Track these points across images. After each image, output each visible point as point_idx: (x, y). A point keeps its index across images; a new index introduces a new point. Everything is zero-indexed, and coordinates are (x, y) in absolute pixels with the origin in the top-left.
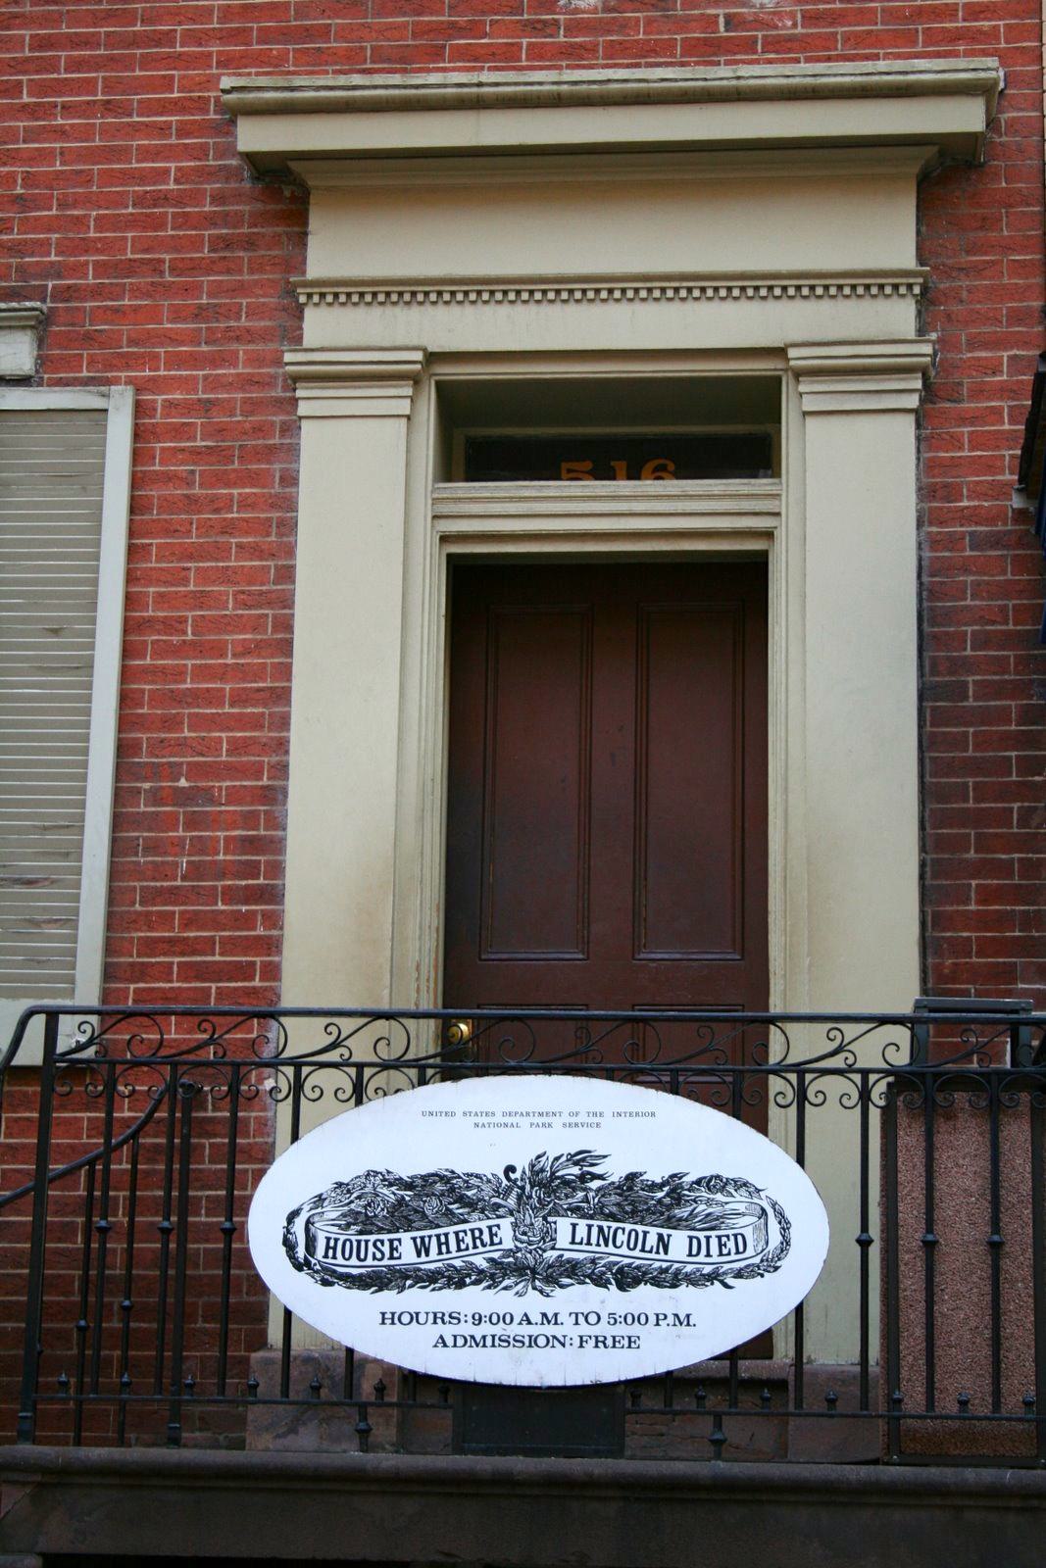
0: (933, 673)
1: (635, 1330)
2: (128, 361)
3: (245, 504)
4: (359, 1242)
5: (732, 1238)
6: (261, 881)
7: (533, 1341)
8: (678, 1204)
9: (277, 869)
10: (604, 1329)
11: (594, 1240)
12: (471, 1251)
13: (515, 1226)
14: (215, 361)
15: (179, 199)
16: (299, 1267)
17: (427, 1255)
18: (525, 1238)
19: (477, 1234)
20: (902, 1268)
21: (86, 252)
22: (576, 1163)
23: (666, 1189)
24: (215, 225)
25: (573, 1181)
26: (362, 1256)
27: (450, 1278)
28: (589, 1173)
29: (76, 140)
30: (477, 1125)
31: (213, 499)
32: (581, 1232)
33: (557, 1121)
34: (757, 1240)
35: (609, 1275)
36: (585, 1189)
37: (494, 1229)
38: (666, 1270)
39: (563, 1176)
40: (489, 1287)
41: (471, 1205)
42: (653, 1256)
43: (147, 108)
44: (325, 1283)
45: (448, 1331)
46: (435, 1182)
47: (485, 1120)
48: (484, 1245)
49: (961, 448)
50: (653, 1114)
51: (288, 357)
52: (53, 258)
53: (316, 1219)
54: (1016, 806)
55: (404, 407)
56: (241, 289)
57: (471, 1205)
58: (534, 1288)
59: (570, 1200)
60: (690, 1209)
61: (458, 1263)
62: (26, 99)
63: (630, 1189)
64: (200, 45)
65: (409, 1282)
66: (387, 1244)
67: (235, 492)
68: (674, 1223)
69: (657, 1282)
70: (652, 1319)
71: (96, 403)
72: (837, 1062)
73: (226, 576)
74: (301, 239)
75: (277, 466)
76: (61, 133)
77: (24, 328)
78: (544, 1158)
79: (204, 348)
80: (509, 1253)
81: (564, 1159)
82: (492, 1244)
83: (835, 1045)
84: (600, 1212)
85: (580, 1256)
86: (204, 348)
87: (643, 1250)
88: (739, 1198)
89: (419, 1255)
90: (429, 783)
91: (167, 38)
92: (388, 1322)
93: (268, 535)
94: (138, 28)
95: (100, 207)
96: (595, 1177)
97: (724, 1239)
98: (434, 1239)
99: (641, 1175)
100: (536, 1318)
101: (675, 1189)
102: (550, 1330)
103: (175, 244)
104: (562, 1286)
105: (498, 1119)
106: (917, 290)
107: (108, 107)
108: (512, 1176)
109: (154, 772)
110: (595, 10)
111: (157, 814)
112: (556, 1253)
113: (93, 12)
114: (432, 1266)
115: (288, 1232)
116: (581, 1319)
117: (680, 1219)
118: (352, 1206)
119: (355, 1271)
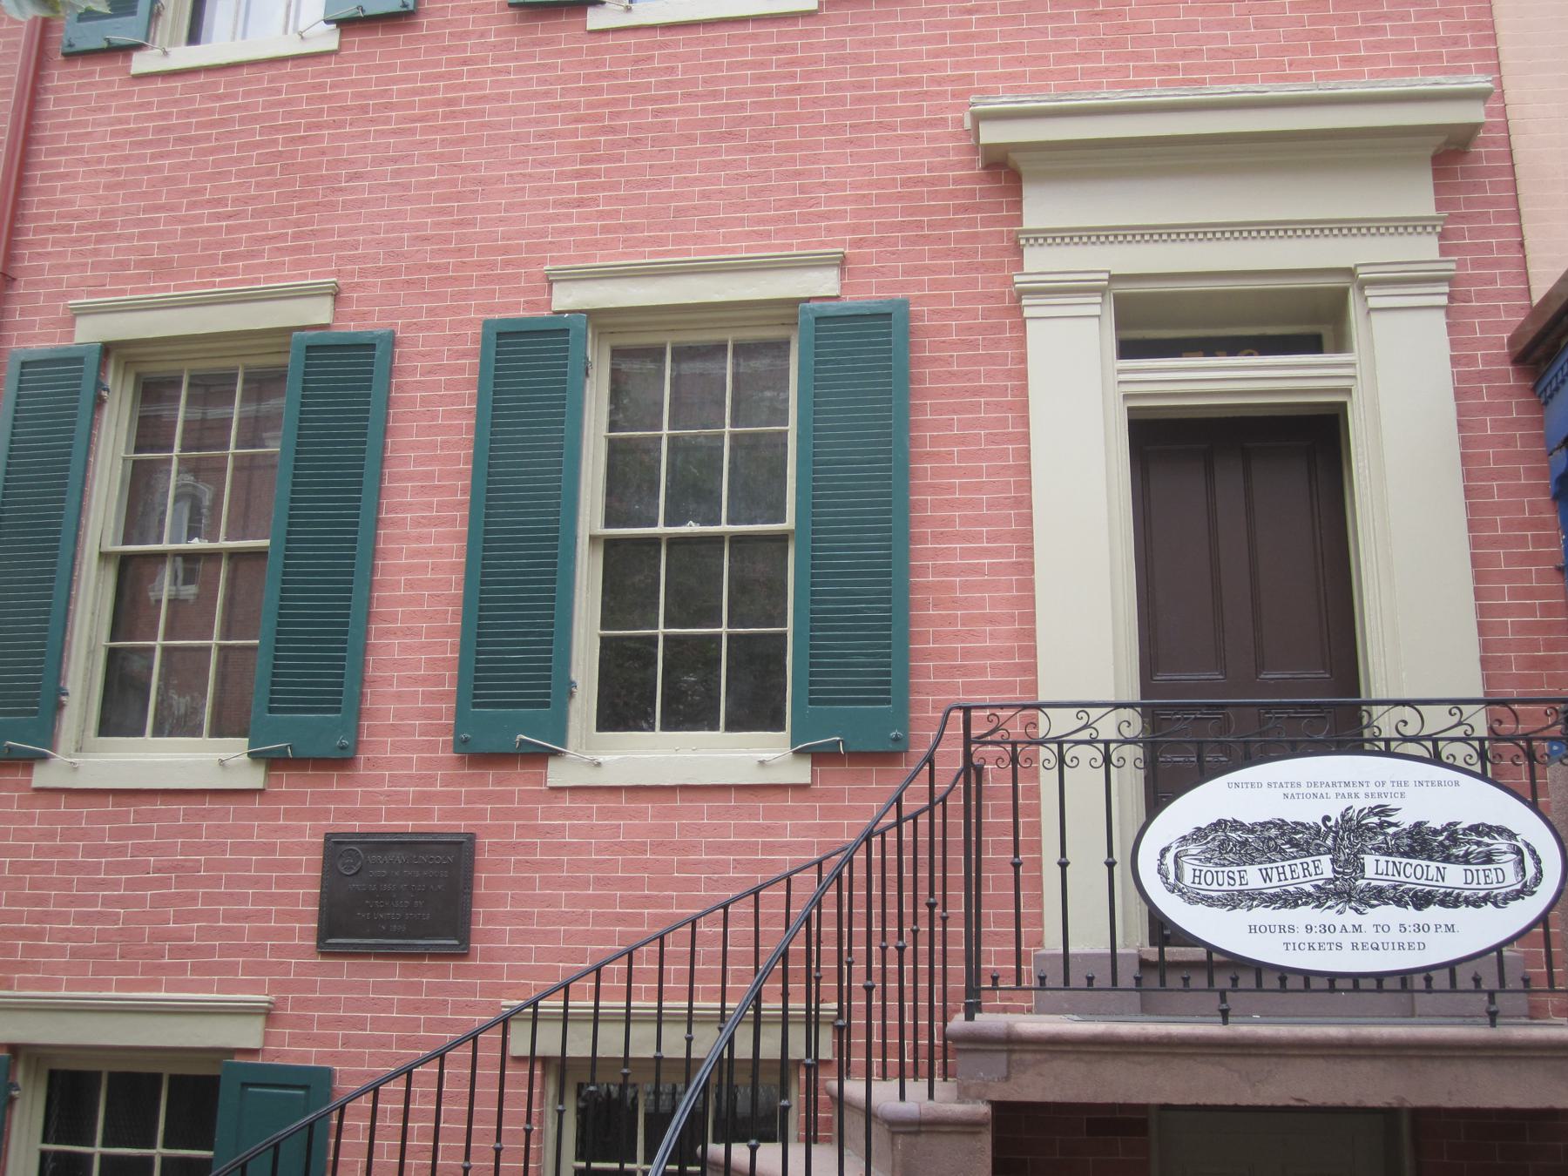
5: (1493, 872)
12: (1302, 879)
13: (1333, 861)
17: (1271, 880)
19: (1305, 866)
22: (1376, 815)
23: (1445, 834)
24: (957, 197)
25: (1374, 828)
27: (1286, 900)
28: (1386, 822)
32: (1382, 866)
35: (1407, 898)
36: (1385, 834)
38: (1450, 894)
39: (1367, 824)
40: (1317, 907)
42: (1434, 883)
46: (1270, 828)
51: (1016, 279)
55: (1096, 310)
58: (1351, 908)
59: (1373, 842)
60: (1465, 848)
61: (1291, 889)
65: (1255, 903)
68: (1447, 859)
69: (1443, 903)
70: (1433, 928)
72: (1084, 735)
74: (1018, 205)
77: (834, 265)
78: (1351, 811)
80: (1329, 881)
82: (1316, 874)
83: (1083, 722)
85: (1384, 884)
89: (1265, 881)
96: (1391, 825)
99: (1425, 823)
104: (1373, 906)
112: (1364, 882)
114: (1272, 891)
115: (1162, 864)
117: (1457, 857)
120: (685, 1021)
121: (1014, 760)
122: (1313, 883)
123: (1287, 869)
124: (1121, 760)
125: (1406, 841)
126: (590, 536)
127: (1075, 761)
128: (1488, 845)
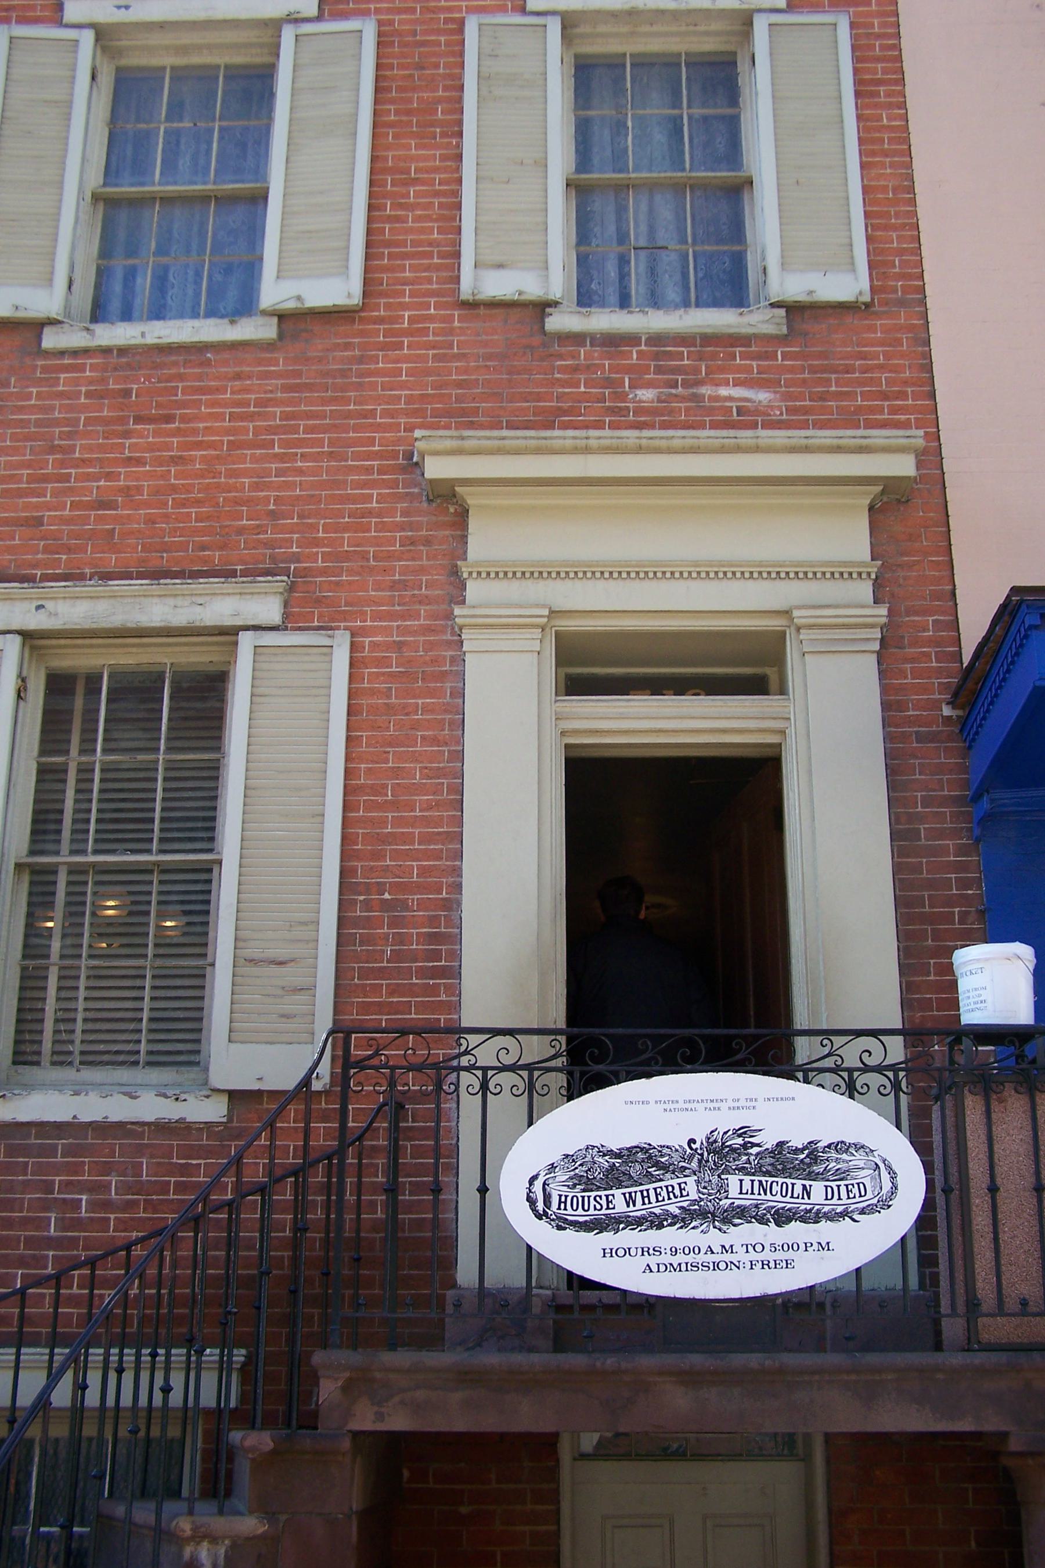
0: (897, 824)
1: (790, 1255)
2: (345, 616)
3: (426, 709)
4: (583, 1197)
5: (856, 1186)
6: (443, 963)
7: (716, 1266)
8: (816, 1163)
9: (456, 955)
10: (768, 1255)
11: (756, 1191)
12: (667, 1202)
13: (698, 1182)
14: (403, 617)
15: (380, 514)
16: (539, 1217)
17: (634, 1205)
18: (705, 1191)
19: (670, 1189)
20: (974, 1208)
21: (317, 546)
22: (740, 1136)
23: (806, 1152)
24: (403, 530)
26: (586, 1208)
27: (652, 1222)
29: (310, 476)
30: (665, 1110)
31: (405, 706)
32: (747, 1186)
33: (724, 1106)
34: (874, 1187)
35: (769, 1216)
37: (683, 1186)
38: (810, 1210)
40: (681, 1228)
41: (665, 1168)
42: (800, 1201)
43: (357, 456)
44: (559, 1228)
45: (653, 1261)
47: (672, 1106)
48: (676, 1197)
49: (906, 678)
50: (793, 1099)
51: (457, 611)
52: (294, 549)
53: (550, 1181)
54: (957, 910)
56: (422, 570)
57: (665, 1168)
58: (715, 1227)
61: (657, 1211)
62: (277, 450)
63: (780, 1153)
64: (393, 418)
65: (622, 1226)
66: (604, 1198)
67: (420, 701)
68: (814, 1177)
69: (804, 1220)
71: (327, 642)
72: (829, 1063)
73: (415, 758)
75: (449, 685)
76: (300, 472)
79: (397, 608)
80: (694, 1202)
81: (730, 1133)
82: (682, 1196)
83: (826, 1050)
84: (759, 1170)
85: (748, 1203)
86: (397, 608)
87: (792, 1197)
88: (859, 1157)
89: (628, 1206)
90: (558, 896)
91: (372, 413)
92: (608, 1255)
93: (443, 730)
94: (352, 407)
95: (326, 518)
96: (754, 1145)
97: (850, 1187)
98: (639, 1194)
100: (717, 1249)
101: (813, 1152)
102: (728, 1257)
103: (377, 542)
104: (735, 1225)
105: (681, 1105)
106: (873, 576)
107: (331, 455)
108: (694, 1146)
109: (367, 889)
110: (652, 402)
111: (368, 917)
112: (729, 1201)
113: (322, 397)
114: (638, 1214)
115: (530, 1191)
116: (750, 1248)
117: (818, 1174)
118: (577, 1171)
119: (581, 1219)
120: (182, 1368)
121: (484, 1087)
122: (679, 1205)
123: (652, 1193)
124: (865, 1087)
125: (769, 1160)
126: (16, 864)
127: (499, 1088)
128: (848, 1162)
